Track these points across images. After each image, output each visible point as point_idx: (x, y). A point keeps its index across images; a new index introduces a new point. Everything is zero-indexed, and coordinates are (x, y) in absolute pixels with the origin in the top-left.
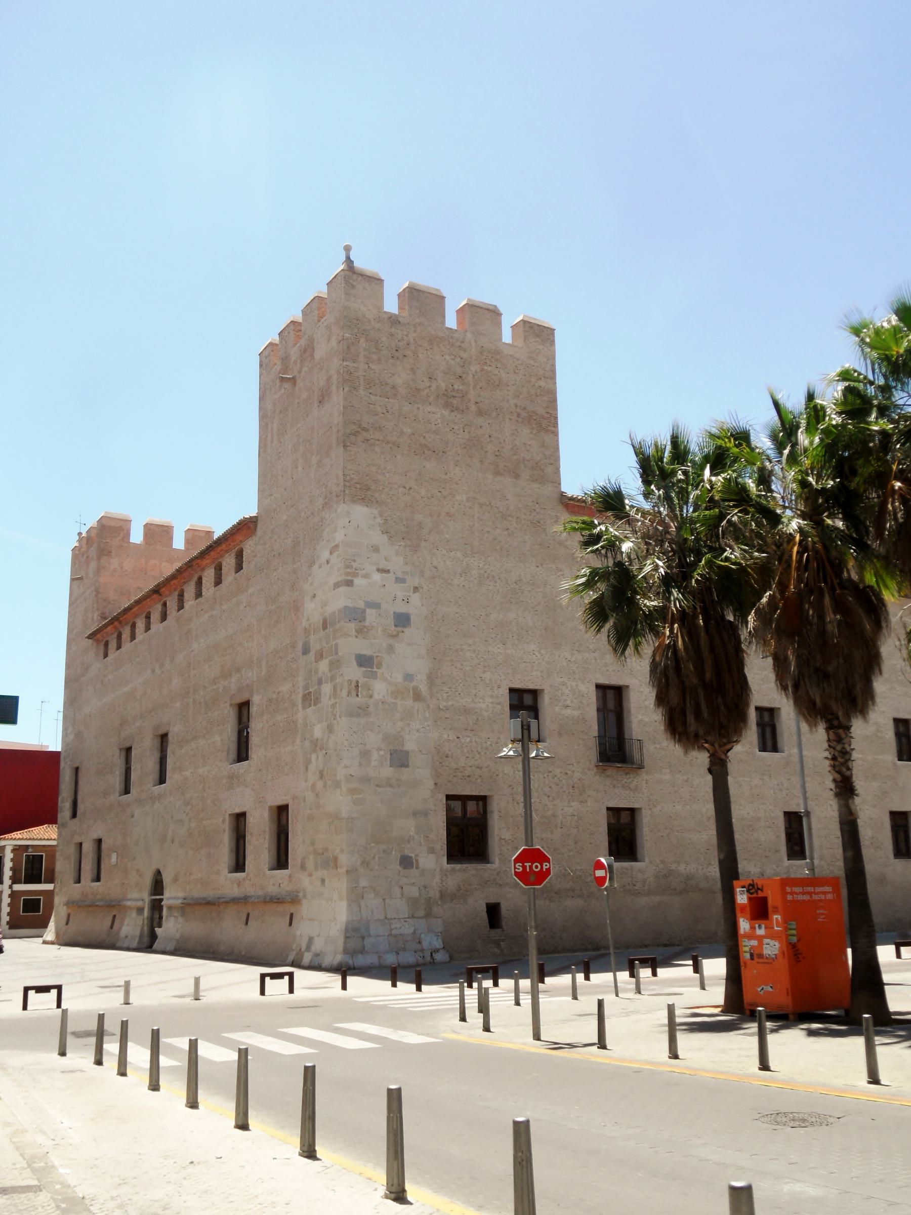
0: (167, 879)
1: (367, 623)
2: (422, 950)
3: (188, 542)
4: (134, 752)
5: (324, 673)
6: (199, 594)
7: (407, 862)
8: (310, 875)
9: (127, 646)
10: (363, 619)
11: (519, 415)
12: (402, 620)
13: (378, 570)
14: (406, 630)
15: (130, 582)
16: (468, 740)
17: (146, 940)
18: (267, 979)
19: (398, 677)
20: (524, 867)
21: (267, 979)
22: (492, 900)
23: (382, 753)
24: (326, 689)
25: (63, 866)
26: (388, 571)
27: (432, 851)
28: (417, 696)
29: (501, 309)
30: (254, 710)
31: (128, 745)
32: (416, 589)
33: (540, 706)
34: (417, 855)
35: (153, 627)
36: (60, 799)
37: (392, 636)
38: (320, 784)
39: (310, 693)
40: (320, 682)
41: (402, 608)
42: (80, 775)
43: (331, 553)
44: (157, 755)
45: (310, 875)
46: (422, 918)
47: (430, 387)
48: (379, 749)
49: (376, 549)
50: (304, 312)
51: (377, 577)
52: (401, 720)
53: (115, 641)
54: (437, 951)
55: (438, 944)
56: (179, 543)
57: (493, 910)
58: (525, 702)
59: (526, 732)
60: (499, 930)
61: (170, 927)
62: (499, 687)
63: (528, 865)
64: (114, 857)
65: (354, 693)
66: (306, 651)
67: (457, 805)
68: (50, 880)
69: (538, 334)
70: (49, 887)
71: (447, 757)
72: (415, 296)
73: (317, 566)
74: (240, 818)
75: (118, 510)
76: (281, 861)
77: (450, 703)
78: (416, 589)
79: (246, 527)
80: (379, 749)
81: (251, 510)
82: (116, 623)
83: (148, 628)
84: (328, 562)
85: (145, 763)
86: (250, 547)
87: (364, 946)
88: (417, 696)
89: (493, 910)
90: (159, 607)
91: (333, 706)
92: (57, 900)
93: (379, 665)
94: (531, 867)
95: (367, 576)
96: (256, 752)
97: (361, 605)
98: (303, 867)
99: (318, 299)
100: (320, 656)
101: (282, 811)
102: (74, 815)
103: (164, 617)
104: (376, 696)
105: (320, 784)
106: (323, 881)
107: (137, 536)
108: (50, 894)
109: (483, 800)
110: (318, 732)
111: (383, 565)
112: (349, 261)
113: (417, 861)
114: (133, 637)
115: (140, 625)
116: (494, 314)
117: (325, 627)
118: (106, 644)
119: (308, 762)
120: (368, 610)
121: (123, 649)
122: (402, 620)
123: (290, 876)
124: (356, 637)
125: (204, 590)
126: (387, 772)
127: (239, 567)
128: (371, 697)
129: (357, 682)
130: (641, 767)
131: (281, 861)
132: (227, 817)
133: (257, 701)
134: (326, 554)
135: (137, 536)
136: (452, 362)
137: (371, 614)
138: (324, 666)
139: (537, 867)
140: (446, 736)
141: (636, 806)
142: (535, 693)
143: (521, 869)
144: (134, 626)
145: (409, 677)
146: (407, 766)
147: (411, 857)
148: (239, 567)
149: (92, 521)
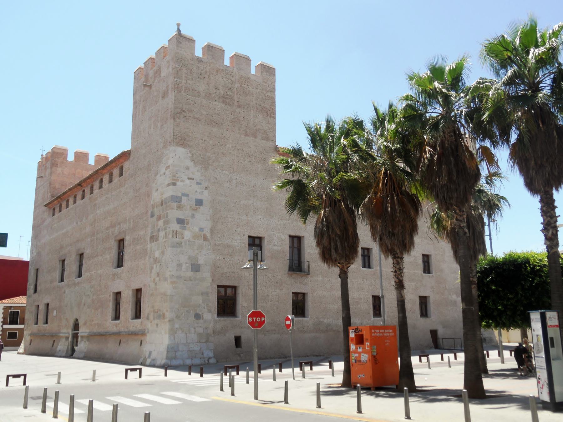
0: (81, 323)
1: (182, 204)
2: (204, 358)
6: (101, 187)
8: (151, 322)
9: (64, 211)
10: (180, 201)
11: (257, 109)
12: (199, 203)
13: (189, 178)
14: (201, 207)
17: (70, 352)
19: (197, 229)
20: (253, 320)
22: (238, 335)
23: (187, 265)
24: (162, 234)
26: (193, 179)
27: (210, 311)
28: (205, 239)
30: (126, 243)
32: (206, 188)
33: (263, 245)
35: (78, 202)
38: (157, 279)
40: (159, 230)
41: (200, 197)
44: (78, 264)
45: (151, 322)
48: (186, 263)
49: (188, 168)
51: (188, 182)
54: (210, 358)
55: (211, 355)
57: (238, 340)
58: (256, 243)
59: (255, 257)
60: (239, 349)
61: (82, 346)
62: (244, 235)
63: (254, 318)
65: (175, 236)
66: (152, 216)
68: (22, 323)
69: (267, 71)
70: (21, 326)
73: (158, 176)
74: (118, 294)
75: (61, 144)
76: (137, 315)
78: (206, 188)
79: (125, 155)
80: (186, 263)
81: (128, 148)
88: (205, 239)
89: (238, 340)
91: (165, 242)
92: (25, 333)
93: (188, 223)
95: (182, 181)
97: (180, 195)
98: (148, 318)
100: (159, 218)
101: (138, 292)
102: (35, 292)
103: (83, 197)
104: (186, 238)
105: (157, 279)
106: (157, 325)
107: (71, 158)
108: (22, 330)
109: (235, 288)
110: (157, 254)
111: (191, 176)
114: (67, 206)
115: (71, 200)
117: (162, 205)
118: (54, 209)
119: (152, 269)
122: (199, 203)
126: (190, 274)
127: (121, 174)
128: (183, 238)
131: (137, 315)
132: (111, 294)
133: (127, 238)
135: (71, 158)
137: (184, 199)
138: (161, 223)
140: (218, 258)
144: (68, 201)
145: (201, 229)
146: (199, 271)
148: (121, 174)
149: (48, 149)
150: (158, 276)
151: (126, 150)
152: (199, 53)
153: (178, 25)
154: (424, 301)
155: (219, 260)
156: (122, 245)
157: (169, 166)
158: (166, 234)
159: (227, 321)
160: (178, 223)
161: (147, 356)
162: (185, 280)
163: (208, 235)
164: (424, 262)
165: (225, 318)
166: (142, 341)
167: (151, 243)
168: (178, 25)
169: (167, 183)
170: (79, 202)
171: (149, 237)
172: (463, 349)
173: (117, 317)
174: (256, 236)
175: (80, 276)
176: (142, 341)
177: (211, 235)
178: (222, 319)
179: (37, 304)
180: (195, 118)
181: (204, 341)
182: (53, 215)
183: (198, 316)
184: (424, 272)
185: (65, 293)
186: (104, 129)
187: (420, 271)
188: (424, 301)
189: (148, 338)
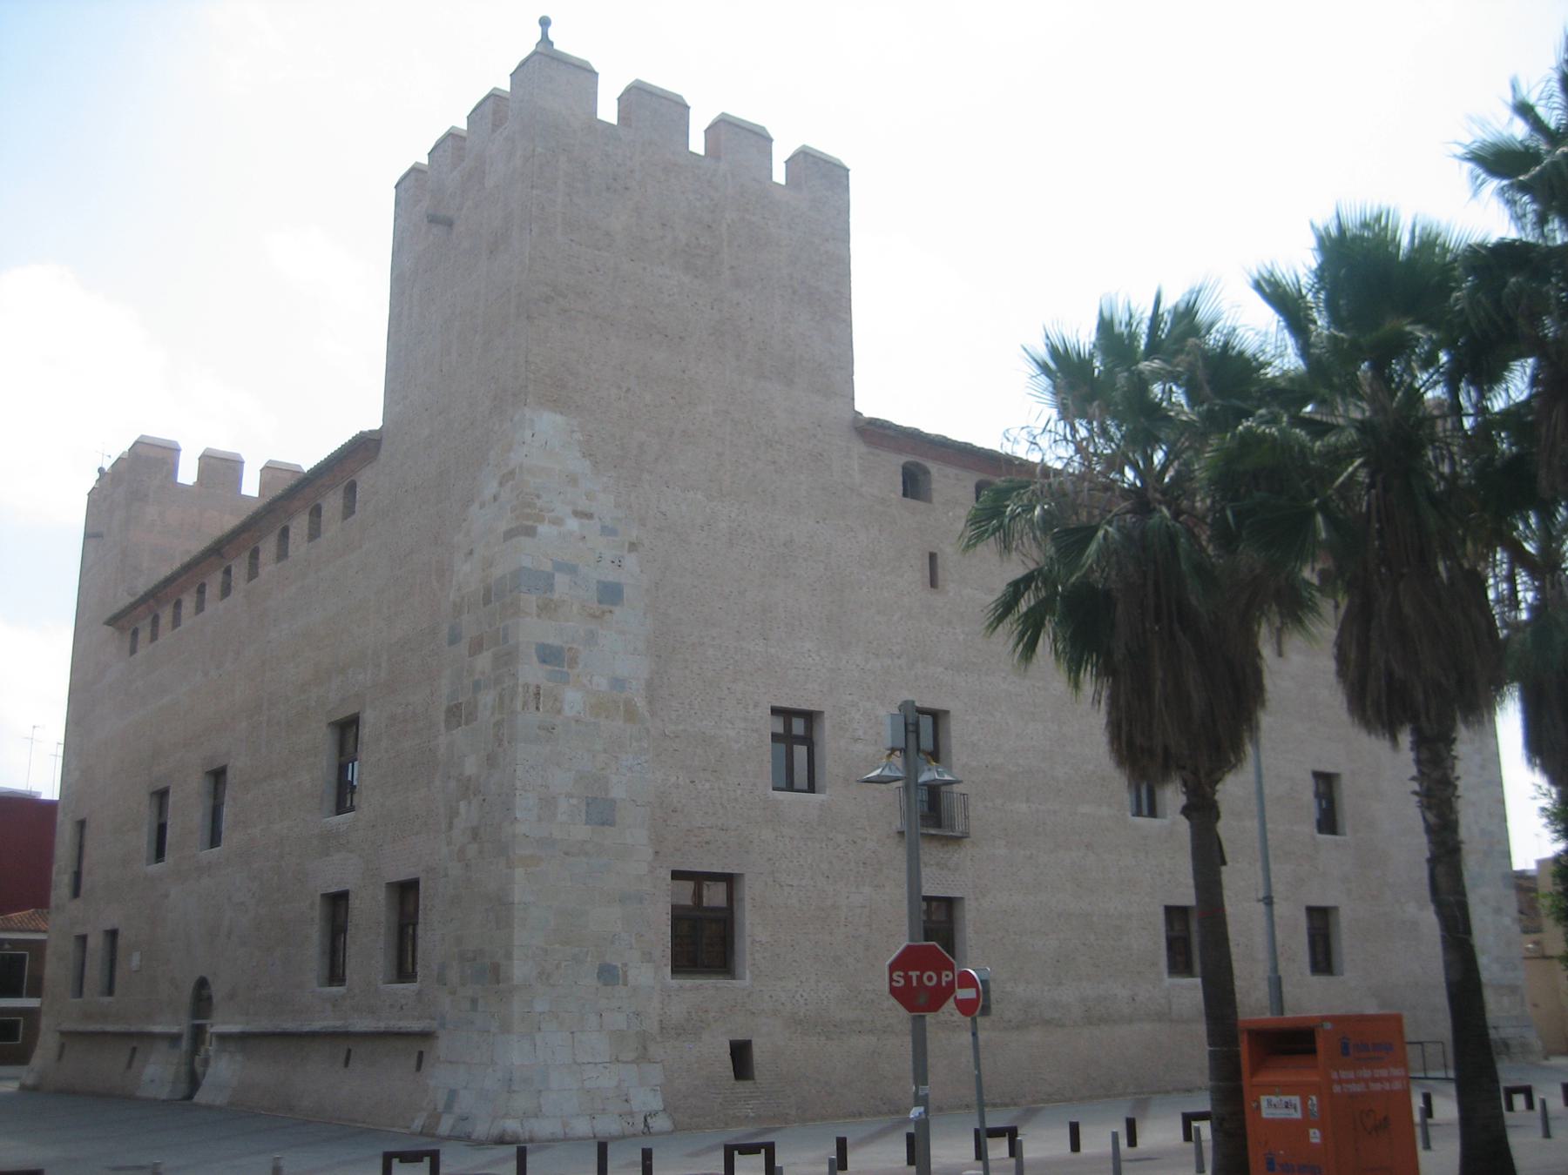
0: (218, 991)
1: (556, 596)
2: (631, 1114)
3: (264, 486)
4: (171, 799)
5: (483, 673)
6: (282, 554)
7: (608, 975)
8: (453, 993)
9: (166, 635)
10: (550, 587)
11: (794, 293)
12: (611, 594)
13: (576, 514)
14: (617, 610)
15: (170, 545)
16: (707, 786)
17: (183, 1088)
18: (395, 1161)
19: (602, 683)
20: (908, 979)
21: (395, 1161)
22: (740, 1036)
23: (574, 801)
24: (487, 698)
25: (55, 970)
26: (589, 516)
27: (647, 957)
28: (631, 714)
29: (772, 133)
30: (365, 732)
31: (161, 786)
32: (633, 547)
33: (816, 737)
34: (625, 965)
35: (209, 608)
36: (55, 868)
37: (594, 616)
38: (472, 849)
39: (458, 706)
40: (477, 686)
41: (611, 576)
42: (87, 831)
43: (501, 484)
44: (209, 803)
45: (453, 993)
46: (632, 1062)
47: (662, 238)
48: (570, 796)
49: (573, 480)
50: (471, 118)
51: (573, 524)
52: (605, 751)
53: (148, 629)
54: (654, 1114)
55: (656, 1103)
56: (251, 486)
57: (741, 1054)
58: (797, 731)
59: (912, 737)
60: (748, 1083)
61: (224, 1073)
62: (756, 706)
63: (914, 974)
64: (136, 959)
65: (532, 706)
66: (454, 639)
67: (689, 886)
68: (36, 992)
69: (822, 176)
70: (33, 1003)
71: (674, 811)
72: (638, 98)
73: (476, 505)
74: (337, 902)
75: (160, 431)
76: (404, 970)
77: (681, 727)
78: (633, 547)
79: (362, 449)
80: (570, 796)
81: (373, 420)
82: (151, 602)
83: (200, 608)
84: (495, 498)
85: (187, 816)
86: (366, 479)
87: (540, 1106)
88: (631, 714)
89: (741, 1054)
90: (218, 577)
91: (498, 724)
92: (44, 1023)
93: (573, 662)
94: (920, 978)
95: (557, 522)
96: (368, 800)
97: (548, 566)
98: (442, 980)
99: (494, 97)
100: (477, 646)
101: (406, 892)
102: (76, 893)
103: (226, 590)
104: (568, 712)
105: (472, 849)
106: (474, 1001)
107: (187, 473)
108: (32, 1015)
109: (729, 880)
110: (471, 767)
111: (584, 504)
112: (545, 40)
113: (625, 973)
114: (176, 622)
115: (189, 603)
116: (759, 139)
117: (487, 601)
118: (135, 633)
119: (453, 813)
120: (557, 575)
121: (160, 641)
122: (611, 594)
123: (419, 993)
124: (539, 616)
125: (291, 547)
126: (581, 831)
127: (349, 510)
128: (559, 712)
129: (538, 687)
130: (957, 840)
131: (404, 970)
132: (318, 899)
133: (369, 719)
134: (492, 487)
135: (187, 473)
136: (698, 204)
137: (561, 580)
138: (484, 661)
139: (930, 979)
140: (673, 779)
141: (957, 894)
142: (810, 717)
143: (902, 982)
144: (178, 605)
145: (618, 683)
146: (612, 824)
147: (615, 967)
148: (349, 510)
149: (121, 446)
150: (474, 839)
151: (366, 429)
152: (608, 111)
153: (545, 23)
154: (1321, 921)
155: (677, 786)
156: (351, 741)
157: (512, 473)
158: (501, 697)
159: (707, 987)
160: (544, 661)
161: (440, 1108)
162: (566, 854)
163: (641, 703)
164: (1318, 795)
165: (699, 982)
166: (421, 1053)
167: (448, 728)
168: (545, 23)
169: (503, 526)
170: (213, 606)
171: (444, 708)
172: (1452, 1074)
173: (335, 974)
174: (795, 706)
175: (215, 839)
176: (421, 1053)
177: (650, 703)
178: (688, 982)
179: (79, 931)
180: (596, 317)
181: (632, 1056)
182: (133, 651)
183: (608, 975)
184: (1321, 831)
185: (166, 896)
186: (297, 379)
187: (1308, 827)
188: (1321, 921)
189: (442, 1047)
